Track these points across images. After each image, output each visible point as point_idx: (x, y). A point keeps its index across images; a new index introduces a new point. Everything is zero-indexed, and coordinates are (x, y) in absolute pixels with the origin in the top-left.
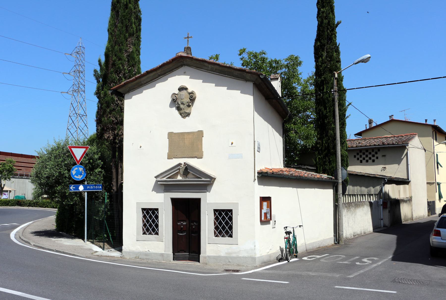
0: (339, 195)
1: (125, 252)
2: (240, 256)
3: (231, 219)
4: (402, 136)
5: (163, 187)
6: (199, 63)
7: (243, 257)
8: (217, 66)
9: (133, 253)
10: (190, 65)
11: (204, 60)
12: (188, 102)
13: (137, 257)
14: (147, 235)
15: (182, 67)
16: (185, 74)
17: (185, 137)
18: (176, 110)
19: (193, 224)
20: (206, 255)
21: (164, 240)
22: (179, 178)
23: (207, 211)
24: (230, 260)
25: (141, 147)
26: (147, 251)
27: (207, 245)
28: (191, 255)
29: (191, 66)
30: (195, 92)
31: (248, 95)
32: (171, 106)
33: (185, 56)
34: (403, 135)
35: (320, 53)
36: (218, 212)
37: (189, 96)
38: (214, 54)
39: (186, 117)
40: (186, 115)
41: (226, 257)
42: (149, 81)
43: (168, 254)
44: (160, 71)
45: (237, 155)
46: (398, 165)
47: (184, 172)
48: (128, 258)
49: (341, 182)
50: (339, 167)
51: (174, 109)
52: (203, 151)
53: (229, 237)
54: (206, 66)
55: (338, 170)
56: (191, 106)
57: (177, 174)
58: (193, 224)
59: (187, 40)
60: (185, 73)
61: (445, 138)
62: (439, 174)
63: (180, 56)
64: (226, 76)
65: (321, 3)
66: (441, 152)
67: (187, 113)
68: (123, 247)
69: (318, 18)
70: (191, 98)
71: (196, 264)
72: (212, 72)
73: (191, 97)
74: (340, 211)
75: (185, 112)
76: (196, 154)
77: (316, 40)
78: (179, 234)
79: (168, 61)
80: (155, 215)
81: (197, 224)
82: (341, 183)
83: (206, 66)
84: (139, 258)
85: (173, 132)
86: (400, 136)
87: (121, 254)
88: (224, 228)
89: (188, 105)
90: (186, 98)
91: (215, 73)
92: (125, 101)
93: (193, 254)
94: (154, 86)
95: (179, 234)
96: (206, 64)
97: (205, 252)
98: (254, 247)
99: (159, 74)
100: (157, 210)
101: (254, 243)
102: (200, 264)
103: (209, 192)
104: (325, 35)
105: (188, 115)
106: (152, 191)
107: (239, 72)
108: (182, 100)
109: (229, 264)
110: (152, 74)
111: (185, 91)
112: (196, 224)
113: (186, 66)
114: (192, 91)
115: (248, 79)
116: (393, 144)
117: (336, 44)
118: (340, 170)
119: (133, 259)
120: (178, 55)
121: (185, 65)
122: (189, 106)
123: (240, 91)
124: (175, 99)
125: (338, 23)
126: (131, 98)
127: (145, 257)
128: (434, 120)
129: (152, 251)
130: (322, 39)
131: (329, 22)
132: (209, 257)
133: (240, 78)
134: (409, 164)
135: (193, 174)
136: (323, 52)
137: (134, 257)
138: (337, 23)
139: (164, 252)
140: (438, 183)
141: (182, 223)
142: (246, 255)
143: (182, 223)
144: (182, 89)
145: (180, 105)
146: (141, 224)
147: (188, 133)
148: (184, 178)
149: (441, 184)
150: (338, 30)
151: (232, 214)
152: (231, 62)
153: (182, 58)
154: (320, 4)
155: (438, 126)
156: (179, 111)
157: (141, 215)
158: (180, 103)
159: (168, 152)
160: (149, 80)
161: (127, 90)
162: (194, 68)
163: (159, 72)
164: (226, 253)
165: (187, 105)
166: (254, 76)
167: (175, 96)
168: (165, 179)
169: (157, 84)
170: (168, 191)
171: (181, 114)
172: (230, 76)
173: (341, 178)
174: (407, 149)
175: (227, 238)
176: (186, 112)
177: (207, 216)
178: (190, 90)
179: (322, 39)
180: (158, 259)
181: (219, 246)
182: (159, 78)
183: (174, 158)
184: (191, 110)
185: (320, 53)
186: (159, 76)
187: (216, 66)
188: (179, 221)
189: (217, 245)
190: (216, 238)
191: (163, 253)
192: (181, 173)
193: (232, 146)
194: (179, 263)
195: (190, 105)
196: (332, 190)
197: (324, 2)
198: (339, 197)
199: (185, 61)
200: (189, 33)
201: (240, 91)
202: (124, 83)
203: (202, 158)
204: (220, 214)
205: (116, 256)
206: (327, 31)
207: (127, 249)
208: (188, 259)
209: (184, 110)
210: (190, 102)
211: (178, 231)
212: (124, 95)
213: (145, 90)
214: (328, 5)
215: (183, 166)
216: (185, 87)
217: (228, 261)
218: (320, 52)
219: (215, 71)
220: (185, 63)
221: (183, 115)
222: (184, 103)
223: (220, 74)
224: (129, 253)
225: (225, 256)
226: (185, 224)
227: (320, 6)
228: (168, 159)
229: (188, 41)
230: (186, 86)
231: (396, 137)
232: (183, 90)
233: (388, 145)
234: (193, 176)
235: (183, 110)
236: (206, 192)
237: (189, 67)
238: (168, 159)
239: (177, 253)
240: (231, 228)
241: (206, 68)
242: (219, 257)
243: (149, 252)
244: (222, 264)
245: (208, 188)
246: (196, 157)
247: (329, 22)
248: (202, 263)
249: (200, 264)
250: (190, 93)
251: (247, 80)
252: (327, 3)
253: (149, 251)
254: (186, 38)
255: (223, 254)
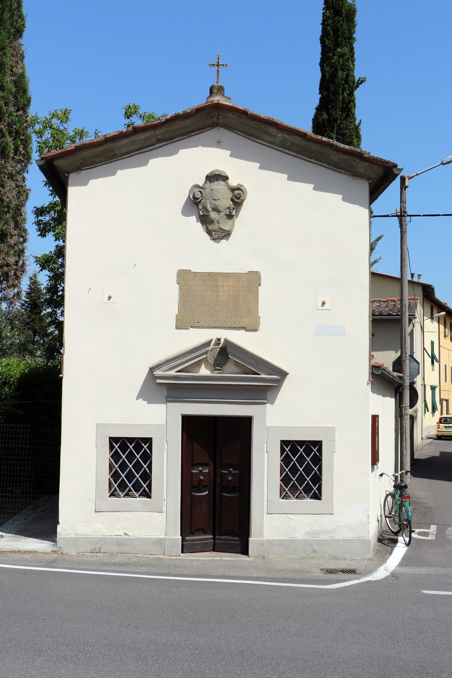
0: (405, 409)
1: (66, 540)
2: (337, 537)
3: (318, 460)
4: (393, 300)
5: (164, 391)
6: (257, 126)
7: (344, 540)
8: (296, 137)
9: (87, 540)
10: (230, 128)
11: (271, 120)
12: (229, 208)
13: (96, 550)
14: (136, 498)
15: (212, 129)
16: (219, 144)
17: (220, 284)
18: (197, 222)
19: (226, 472)
20: (263, 538)
21: (164, 508)
22: (204, 371)
23: (265, 444)
24: (316, 548)
25: (110, 298)
26: (123, 535)
27: (266, 516)
28: (220, 539)
29: (234, 129)
30: (245, 188)
31: (357, 206)
32: (186, 212)
33: (229, 106)
34: (395, 299)
35: (326, 134)
36: (290, 446)
37: (230, 195)
38: (59, 107)
39: (221, 239)
40: (223, 235)
41: (307, 541)
42: (133, 151)
43: (175, 539)
44: (162, 130)
45: (333, 328)
46: (396, 353)
47: (216, 360)
48: (74, 553)
49: (408, 384)
50: (406, 357)
51: (193, 219)
52: (259, 315)
53: (311, 498)
54: (270, 135)
55: (404, 362)
56: (235, 217)
57: (198, 364)
58: (226, 472)
59: (216, 72)
60: (219, 142)
61: (430, 307)
62: (434, 371)
63: (216, 103)
64: (313, 160)
65: (334, 37)
66: (433, 332)
67: (226, 231)
68: (59, 529)
69: (325, 65)
70: (236, 200)
71: (239, 559)
72: (281, 149)
73: (236, 198)
74: (406, 439)
75: (220, 228)
76: (244, 321)
77: (319, 109)
78: (194, 494)
79: (189, 111)
80: (142, 452)
81: (239, 472)
82: (408, 387)
83: (270, 135)
84: (102, 551)
85: (190, 270)
86: (391, 300)
87: (54, 545)
88: (130, 476)
89: (228, 213)
90: (225, 199)
91: (287, 151)
92: (69, 187)
93: (224, 537)
94: (146, 164)
95: (194, 494)
96: (272, 130)
97: (261, 533)
98: (367, 518)
99: (159, 137)
100: (148, 441)
101: (368, 510)
102: (251, 559)
103: (272, 403)
104: (338, 101)
105: (227, 235)
106: (138, 398)
107: (345, 157)
108: (217, 203)
109: (313, 555)
110: (142, 136)
111: (222, 183)
112: (233, 472)
113: (222, 127)
114: (239, 184)
115: (359, 173)
116: (390, 315)
117: (354, 122)
118: (407, 361)
119: (87, 554)
120: (212, 101)
121: (220, 126)
122: (230, 217)
123: (341, 196)
124: (199, 198)
125: (361, 81)
126: (85, 183)
127: (115, 549)
128: (418, 275)
129: (135, 533)
130: (332, 107)
131: (347, 76)
132: (269, 542)
133: (342, 169)
134: (415, 352)
135: (237, 364)
136: (332, 134)
137: (89, 550)
138: (358, 81)
139: (164, 536)
140: (433, 387)
141: (201, 469)
142: (349, 535)
143: (201, 470)
144: (216, 177)
145: (209, 212)
146: (106, 476)
147: (227, 275)
148: (216, 372)
149: (436, 388)
150: (357, 93)
151: (150, 447)
152: (96, 130)
153: (218, 110)
154: (331, 37)
155: (432, 286)
156: (205, 226)
157: (107, 455)
158: (209, 208)
159: (176, 312)
160: (133, 148)
161: (78, 164)
162: (241, 135)
163: (159, 133)
164: (307, 532)
165: (226, 215)
166: (376, 167)
167: (201, 192)
168: (173, 373)
169: (151, 160)
170: (177, 399)
171: (209, 232)
172: (321, 162)
173: (408, 378)
174: (413, 324)
175: (308, 501)
176: (223, 230)
177: (266, 454)
178: (233, 182)
179: (332, 107)
180: (150, 553)
181: (292, 519)
182: (157, 146)
183: (191, 327)
184: (233, 226)
185: (326, 134)
186: (159, 141)
187: (294, 136)
188: (195, 465)
189: (288, 517)
190: (283, 500)
191: (162, 538)
192: (210, 362)
193: (323, 308)
194: (201, 558)
195: (233, 214)
196: (393, 400)
197: (338, 37)
198: (404, 413)
199: (222, 117)
200: (220, 54)
201: (341, 196)
202: (75, 147)
203: (256, 330)
204: (124, 448)
205: (39, 550)
206: (343, 94)
207: (69, 532)
208: (212, 548)
209: (220, 225)
210: (234, 209)
211: (193, 487)
212: (67, 175)
213: (121, 170)
214: (346, 43)
215: (213, 348)
216: (225, 175)
217: (311, 550)
218: (326, 133)
219: (288, 148)
220: (221, 121)
221: (215, 234)
222: (221, 209)
223: (298, 155)
224: (75, 541)
225: (305, 540)
226: (207, 471)
227: (330, 41)
228: (177, 328)
229: (218, 73)
230: (225, 173)
231: (383, 301)
232: (217, 180)
233: (380, 315)
234: (236, 369)
235: (217, 223)
236: (265, 403)
237: (229, 130)
238: (177, 328)
239: (189, 536)
240: (317, 479)
241: (270, 139)
242: (292, 541)
243: (127, 537)
244: (297, 558)
245: (269, 395)
246: (244, 328)
247: (347, 76)
248: (255, 557)
249: (251, 559)
250: (233, 190)
251: (356, 174)
252: (345, 39)
253: (126, 534)
254: (213, 65)
255: (300, 536)
